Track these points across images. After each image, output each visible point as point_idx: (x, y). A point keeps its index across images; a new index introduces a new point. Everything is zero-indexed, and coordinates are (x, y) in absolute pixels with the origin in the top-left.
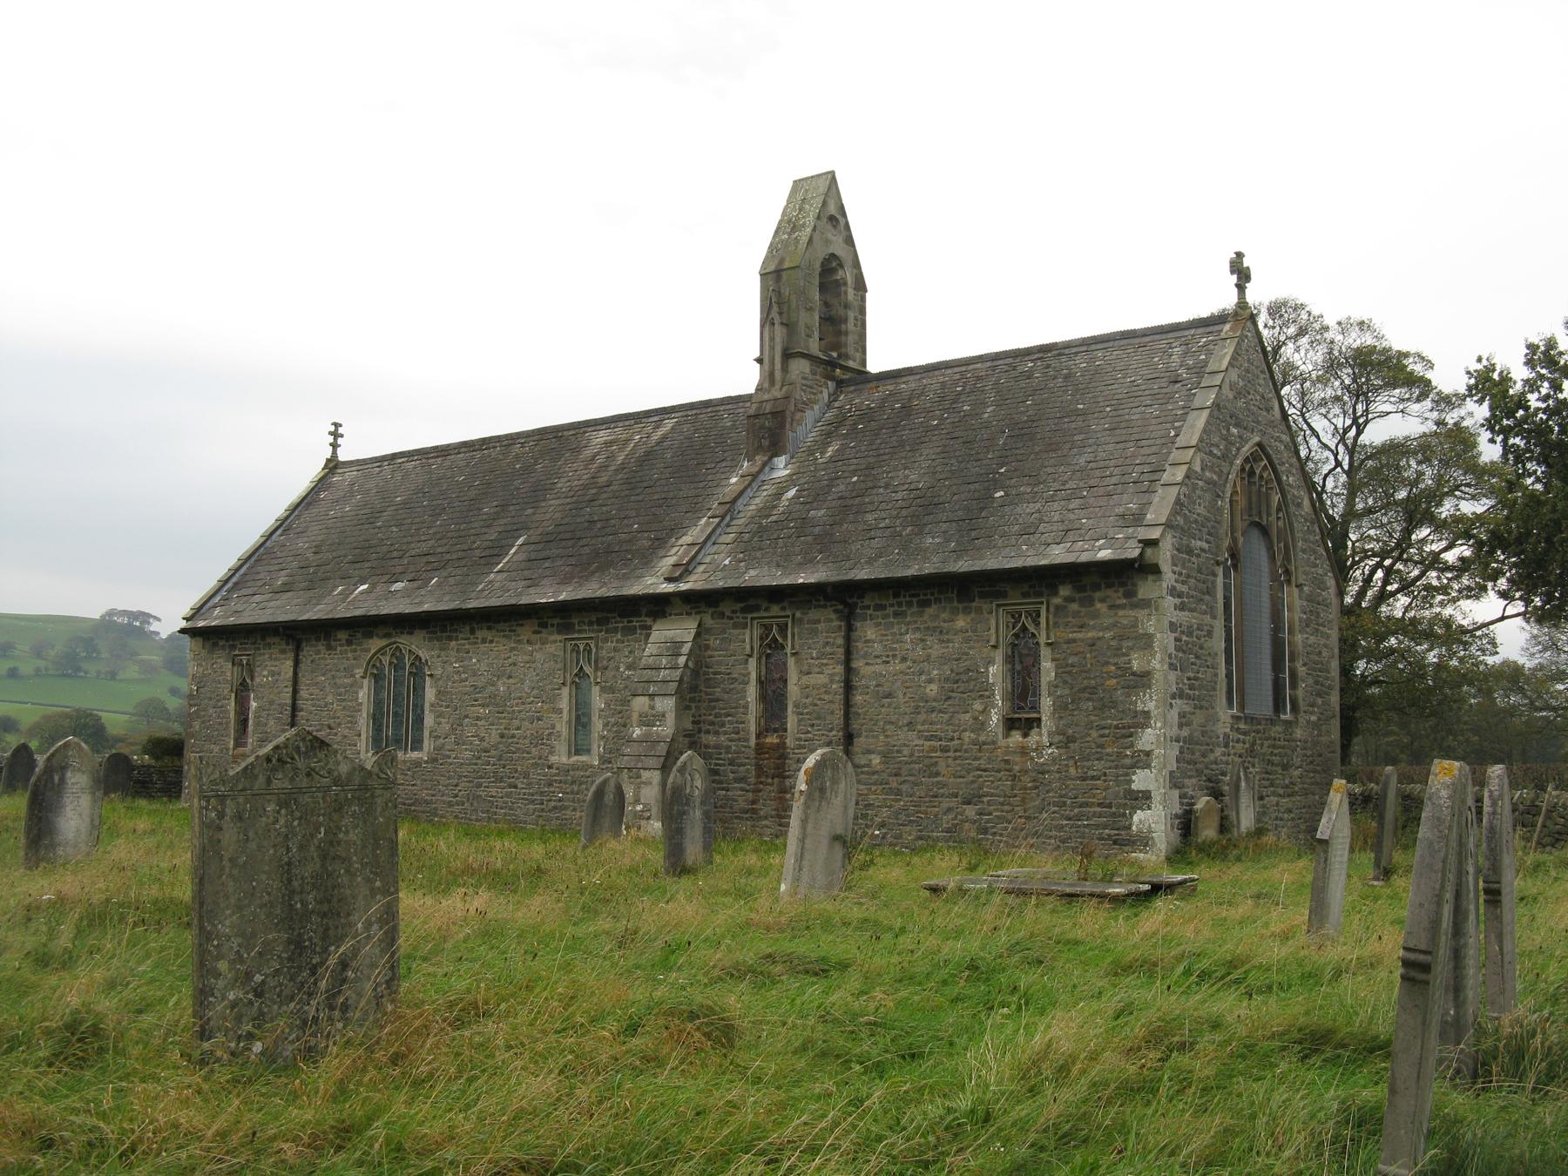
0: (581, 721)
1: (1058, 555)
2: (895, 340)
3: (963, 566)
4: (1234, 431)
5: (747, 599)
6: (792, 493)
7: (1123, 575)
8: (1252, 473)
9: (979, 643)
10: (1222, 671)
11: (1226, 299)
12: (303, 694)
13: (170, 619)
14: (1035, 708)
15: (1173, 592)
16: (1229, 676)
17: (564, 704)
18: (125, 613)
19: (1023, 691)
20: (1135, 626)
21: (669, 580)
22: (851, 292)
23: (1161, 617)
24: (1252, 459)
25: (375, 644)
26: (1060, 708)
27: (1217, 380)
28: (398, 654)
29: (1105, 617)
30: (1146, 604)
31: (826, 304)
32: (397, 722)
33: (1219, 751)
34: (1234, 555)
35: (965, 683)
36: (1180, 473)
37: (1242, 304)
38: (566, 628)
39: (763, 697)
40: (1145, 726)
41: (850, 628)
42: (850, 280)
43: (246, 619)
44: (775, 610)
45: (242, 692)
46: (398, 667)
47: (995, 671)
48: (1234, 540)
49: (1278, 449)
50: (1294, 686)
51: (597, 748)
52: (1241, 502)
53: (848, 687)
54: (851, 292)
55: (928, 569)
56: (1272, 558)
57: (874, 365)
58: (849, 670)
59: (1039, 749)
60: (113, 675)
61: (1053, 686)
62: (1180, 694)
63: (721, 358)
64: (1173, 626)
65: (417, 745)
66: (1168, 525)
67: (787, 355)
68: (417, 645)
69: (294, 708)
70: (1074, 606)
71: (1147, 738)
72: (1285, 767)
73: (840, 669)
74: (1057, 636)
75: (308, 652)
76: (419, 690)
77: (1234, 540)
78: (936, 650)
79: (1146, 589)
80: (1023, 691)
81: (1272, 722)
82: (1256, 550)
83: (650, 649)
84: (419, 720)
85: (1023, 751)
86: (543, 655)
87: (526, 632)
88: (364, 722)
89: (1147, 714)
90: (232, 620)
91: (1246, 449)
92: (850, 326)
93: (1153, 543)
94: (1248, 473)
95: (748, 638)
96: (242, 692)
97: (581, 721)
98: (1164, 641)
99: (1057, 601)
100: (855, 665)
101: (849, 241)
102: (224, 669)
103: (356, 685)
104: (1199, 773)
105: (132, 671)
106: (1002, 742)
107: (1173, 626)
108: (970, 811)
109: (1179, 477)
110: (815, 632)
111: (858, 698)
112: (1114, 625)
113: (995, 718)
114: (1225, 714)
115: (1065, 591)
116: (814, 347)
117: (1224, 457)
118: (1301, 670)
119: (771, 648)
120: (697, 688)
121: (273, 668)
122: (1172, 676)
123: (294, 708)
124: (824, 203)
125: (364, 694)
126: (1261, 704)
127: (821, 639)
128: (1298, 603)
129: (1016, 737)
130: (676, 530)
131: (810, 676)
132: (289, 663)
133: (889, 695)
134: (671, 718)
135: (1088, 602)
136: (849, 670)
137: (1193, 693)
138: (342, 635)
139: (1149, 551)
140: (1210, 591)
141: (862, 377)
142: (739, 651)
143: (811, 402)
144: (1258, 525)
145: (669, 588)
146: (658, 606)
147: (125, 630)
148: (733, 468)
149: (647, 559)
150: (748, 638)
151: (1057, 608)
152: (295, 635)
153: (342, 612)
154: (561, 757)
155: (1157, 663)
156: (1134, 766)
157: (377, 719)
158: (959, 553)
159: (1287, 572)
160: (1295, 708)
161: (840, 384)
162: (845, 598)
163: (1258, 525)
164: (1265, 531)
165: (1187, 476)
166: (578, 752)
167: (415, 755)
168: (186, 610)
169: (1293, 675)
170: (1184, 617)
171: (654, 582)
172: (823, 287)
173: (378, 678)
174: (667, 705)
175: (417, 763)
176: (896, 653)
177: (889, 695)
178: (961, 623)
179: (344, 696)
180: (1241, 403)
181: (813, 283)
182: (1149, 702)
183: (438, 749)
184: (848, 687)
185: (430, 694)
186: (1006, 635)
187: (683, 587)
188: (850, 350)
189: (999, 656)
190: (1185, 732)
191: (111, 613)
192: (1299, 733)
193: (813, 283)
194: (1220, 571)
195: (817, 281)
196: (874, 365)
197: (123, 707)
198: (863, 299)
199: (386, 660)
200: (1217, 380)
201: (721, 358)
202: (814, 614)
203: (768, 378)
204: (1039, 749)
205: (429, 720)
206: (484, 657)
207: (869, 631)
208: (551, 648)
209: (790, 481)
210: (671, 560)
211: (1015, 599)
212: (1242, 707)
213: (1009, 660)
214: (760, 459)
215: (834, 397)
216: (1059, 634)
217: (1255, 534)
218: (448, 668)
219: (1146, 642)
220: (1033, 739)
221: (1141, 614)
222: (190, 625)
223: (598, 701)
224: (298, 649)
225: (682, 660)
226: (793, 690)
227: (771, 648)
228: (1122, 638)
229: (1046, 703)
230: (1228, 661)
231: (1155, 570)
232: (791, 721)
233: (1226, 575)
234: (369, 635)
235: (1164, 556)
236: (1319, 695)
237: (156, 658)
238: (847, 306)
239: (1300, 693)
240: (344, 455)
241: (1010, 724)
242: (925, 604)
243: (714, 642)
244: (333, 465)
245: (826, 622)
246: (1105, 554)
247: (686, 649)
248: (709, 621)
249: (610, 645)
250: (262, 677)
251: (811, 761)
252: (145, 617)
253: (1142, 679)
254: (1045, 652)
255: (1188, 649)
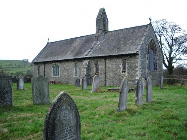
0: (76, 72)
1: (127, 53)
2: (112, 27)
3: (117, 54)
4: (149, 38)
5: (94, 58)
6: (99, 45)
7: (135, 55)
8: (151, 43)
9: (119, 63)
10: (147, 65)
11: (148, 23)
12: (46, 69)
13: (30, 61)
14: (125, 70)
15: (140, 57)
16: (148, 66)
17: (74, 70)
18: (25, 60)
19: (124, 68)
20: (136, 61)
21: (86, 56)
22: (106, 22)
23: (139, 59)
24: (152, 41)
25: (53, 64)
26: (128, 70)
27: (147, 32)
28: (56, 65)
29: (133, 60)
30: (137, 58)
31: (104, 23)
32: (56, 73)
33: (146, 74)
34: (149, 52)
35: (118, 67)
36: (141, 43)
37: (150, 23)
38: (74, 61)
39: (96, 69)
40: (137, 72)
41: (105, 61)
42: (106, 20)
43: (39, 61)
44: (97, 59)
45: (39, 70)
46: (56, 66)
47: (121, 66)
48: (149, 50)
49: (155, 40)
50: (157, 67)
51: (78, 75)
52: (150, 46)
53: (105, 68)
54: (106, 22)
55: (114, 54)
56: (154, 52)
57: (110, 30)
58: (105, 66)
59: (126, 74)
60: (24, 67)
61: (52, 71)
62: (141, 68)
63: (91, 29)
64: (140, 61)
65: (58, 75)
66: (140, 49)
67: (99, 30)
68: (58, 64)
69: (45, 71)
70: (129, 58)
71: (137, 73)
72: (155, 76)
73: (104, 66)
74: (128, 62)
75: (46, 65)
76: (58, 69)
77: (149, 50)
78: (115, 64)
79: (137, 57)
80: (124, 68)
81: (154, 71)
82: (152, 52)
83: (84, 64)
84: (58, 72)
85: (124, 75)
86: (72, 64)
87: (70, 62)
88: (52, 72)
89: (137, 70)
90: (37, 62)
91: (150, 40)
92: (106, 25)
93: (138, 51)
94: (150, 43)
95: (94, 62)
96: (39, 70)
97: (76, 72)
98: (139, 62)
99: (128, 58)
100: (106, 65)
101: (106, 16)
102: (36, 67)
103: (51, 68)
104: (144, 77)
105: (26, 67)
106: (122, 74)
107: (140, 61)
108: (118, 81)
109: (141, 44)
110: (102, 62)
111: (106, 69)
112: (134, 61)
113: (121, 71)
114: (147, 70)
115: (128, 57)
116: (102, 28)
117: (147, 41)
118: (158, 65)
119: (97, 63)
120: (89, 68)
121: (42, 67)
122: (140, 66)
123: (45, 71)
124: (103, 12)
125: (52, 69)
126: (152, 69)
127: (102, 62)
128: (157, 57)
129: (123, 73)
130: (86, 50)
131: (101, 66)
132: (44, 66)
133: (110, 68)
134: (86, 71)
135: (131, 58)
136: (105, 66)
137: (143, 68)
138: (50, 63)
139: (137, 52)
140: (145, 57)
141: (108, 32)
142: (93, 63)
143: (102, 35)
144: (152, 49)
145: (86, 57)
146: (84, 59)
147: (25, 62)
148: (93, 43)
149: (83, 53)
150: (94, 62)
151: (128, 59)
152: (45, 63)
153: (49, 60)
154: (74, 76)
155: (139, 65)
156: (136, 76)
157: (54, 72)
158: (118, 52)
159: (156, 54)
160: (157, 70)
161: (105, 32)
162: (105, 58)
163: (152, 49)
164: (153, 49)
165: (142, 43)
166: (76, 75)
167: (58, 76)
168: (32, 60)
169: (157, 66)
170: (142, 59)
171: (84, 56)
172: (103, 21)
173: (54, 68)
174: (85, 70)
175: (58, 77)
176: (110, 63)
177: (110, 68)
178: (117, 60)
179: (50, 69)
180: (150, 35)
181: (102, 19)
182: (137, 69)
183: (61, 75)
184: (105, 68)
185: (60, 69)
186: (122, 62)
187: (87, 57)
188: (107, 28)
189: (121, 64)
190: (142, 72)
191: (24, 60)
192: (157, 72)
193: (102, 19)
194: (147, 54)
195: (102, 21)
196: (110, 30)
197: (25, 71)
198: (108, 22)
199: (55, 65)
200: (147, 32)
201: (91, 29)
202: (101, 60)
203: (97, 32)
204: (126, 74)
205: (59, 72)
206: (65, 65)
207: (107, 61)
208: (73, 64)
209: (99, 44)
210: (86, 54)
211: (123, 58)
212: (150, 69)
213: (123, 64)
214: (96, 42)
215: (104, 34)
216: (128, 62)
217: (152, 50)
218: (61, 66)
219: (137, 62)
220: (125, 73)
221: (137, 59)
222: (33, 62)
223: (78, 70)
224: (45, 65)
225: (87, 65)
226: (99, 68)
227: (97, 63)
228: (135, 62)
229: (127, 69)
230: (148, 64)
231: (138, 54)
232: (99, 72)
233: (148, 54)
234: (53, 63)
235: (139, 53)
236: (160, 68)
237: (30, 65)
238: (106, 23)
239: (157, 68)
240: (49, 42)
241: (123, 72)
242: (113, 58)
243: (91, 63)
244: (48, 43)
245: (102, 61)
246: (133, 53)
247: (87, 64)
248: (90, 60)
249: (79, 63)
250: (41, 68)
251: (95, 76)
252: (28, 60)
253: (137, 67)
254: (126, 63)
255: (142, 63)
